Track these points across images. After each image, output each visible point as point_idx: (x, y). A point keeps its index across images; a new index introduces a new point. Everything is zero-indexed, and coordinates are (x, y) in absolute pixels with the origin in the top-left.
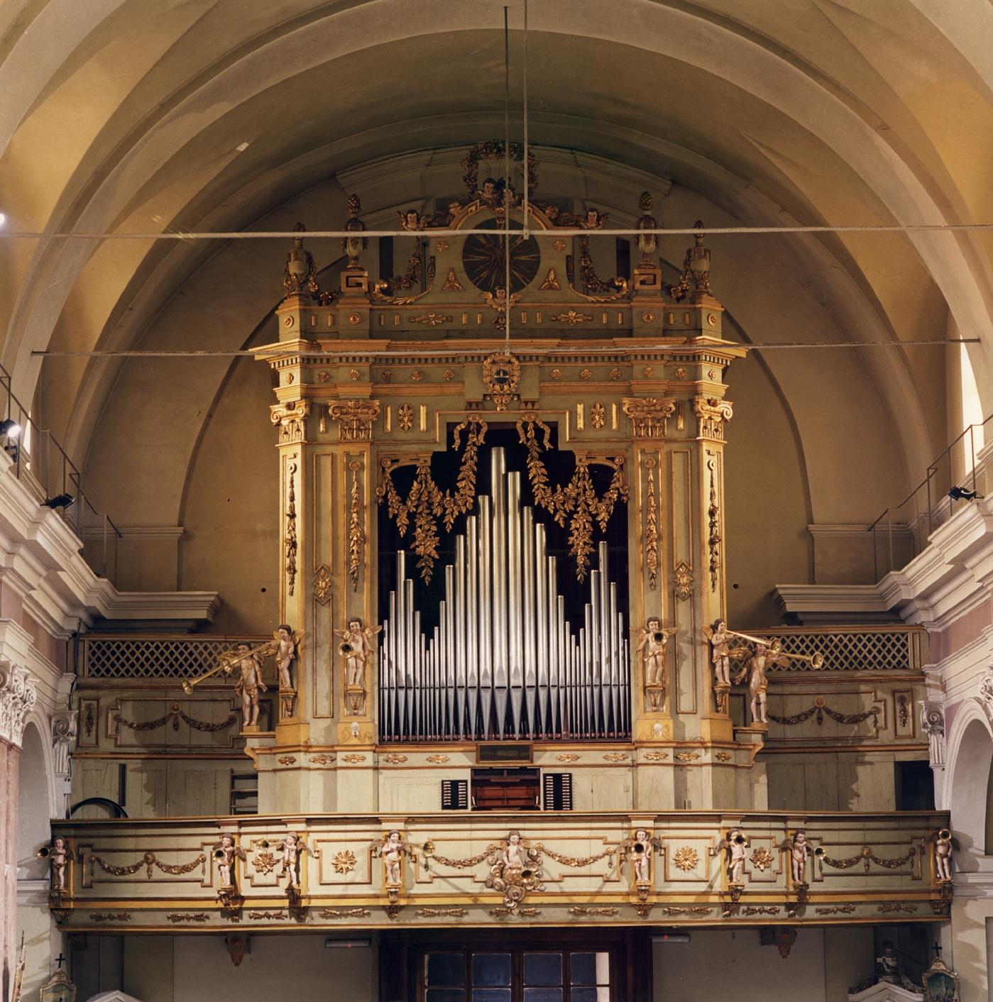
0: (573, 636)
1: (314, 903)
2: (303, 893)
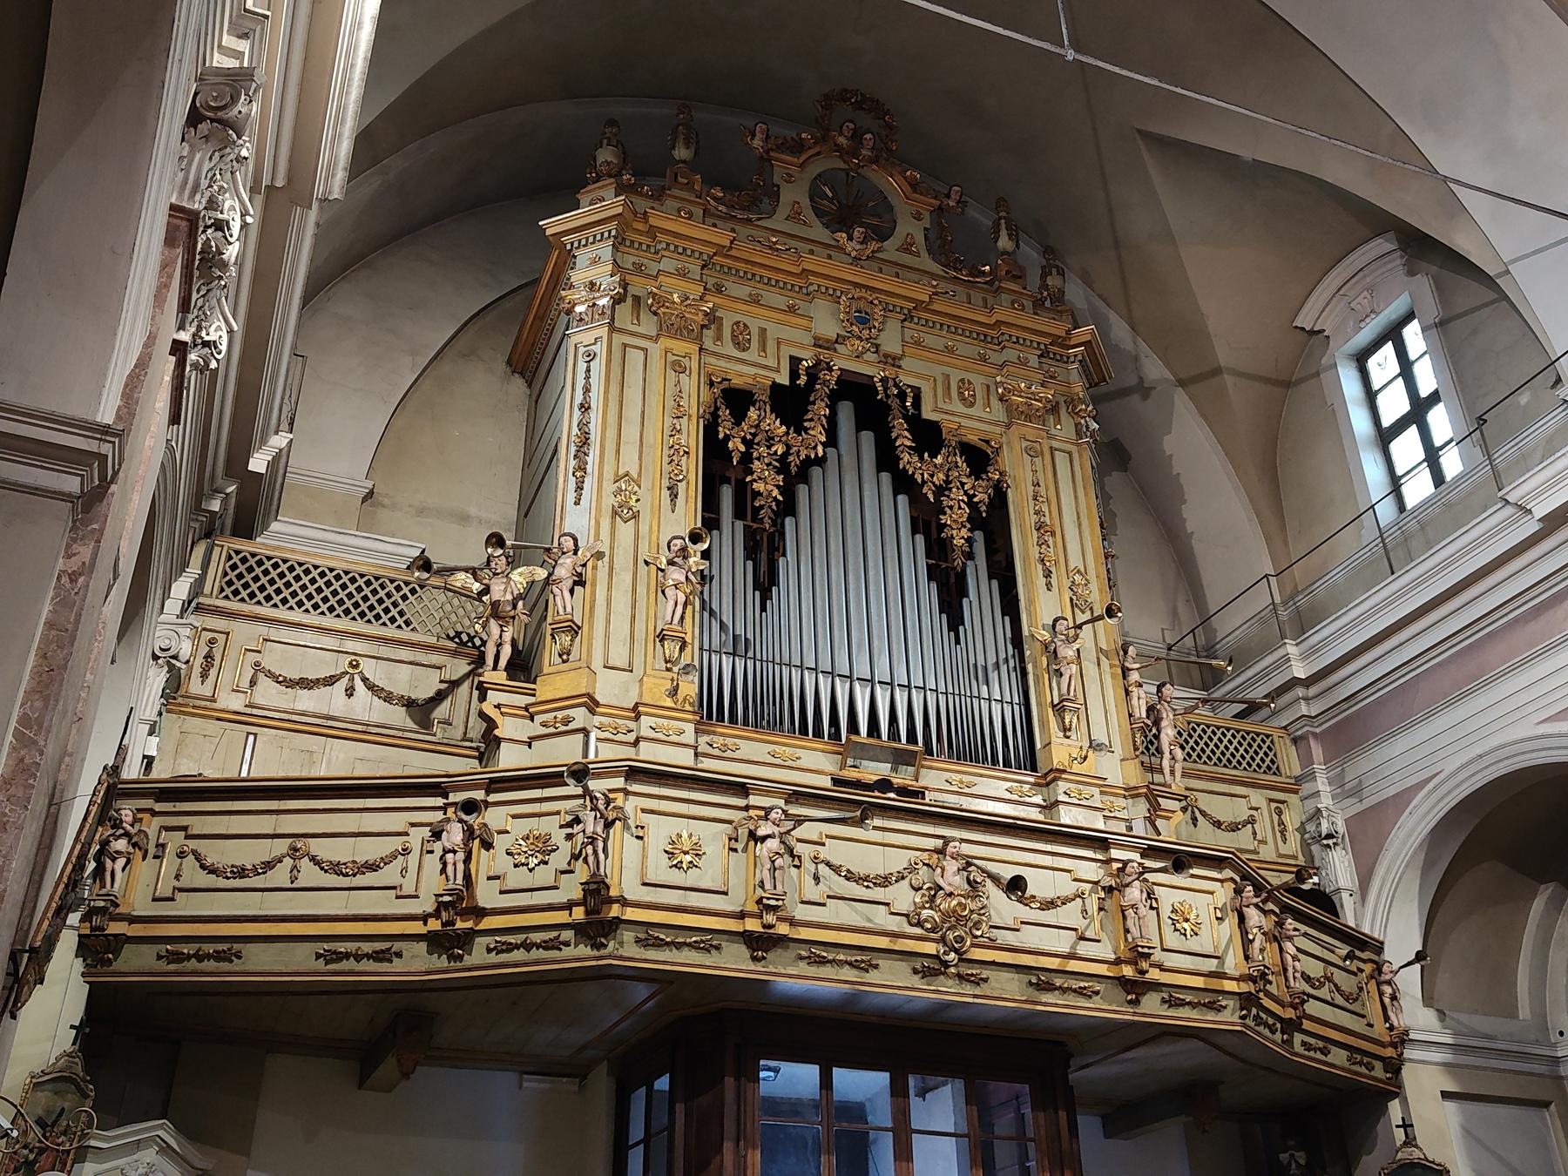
0: (952, 634)
1: (631, 914)
2: (613, 892)
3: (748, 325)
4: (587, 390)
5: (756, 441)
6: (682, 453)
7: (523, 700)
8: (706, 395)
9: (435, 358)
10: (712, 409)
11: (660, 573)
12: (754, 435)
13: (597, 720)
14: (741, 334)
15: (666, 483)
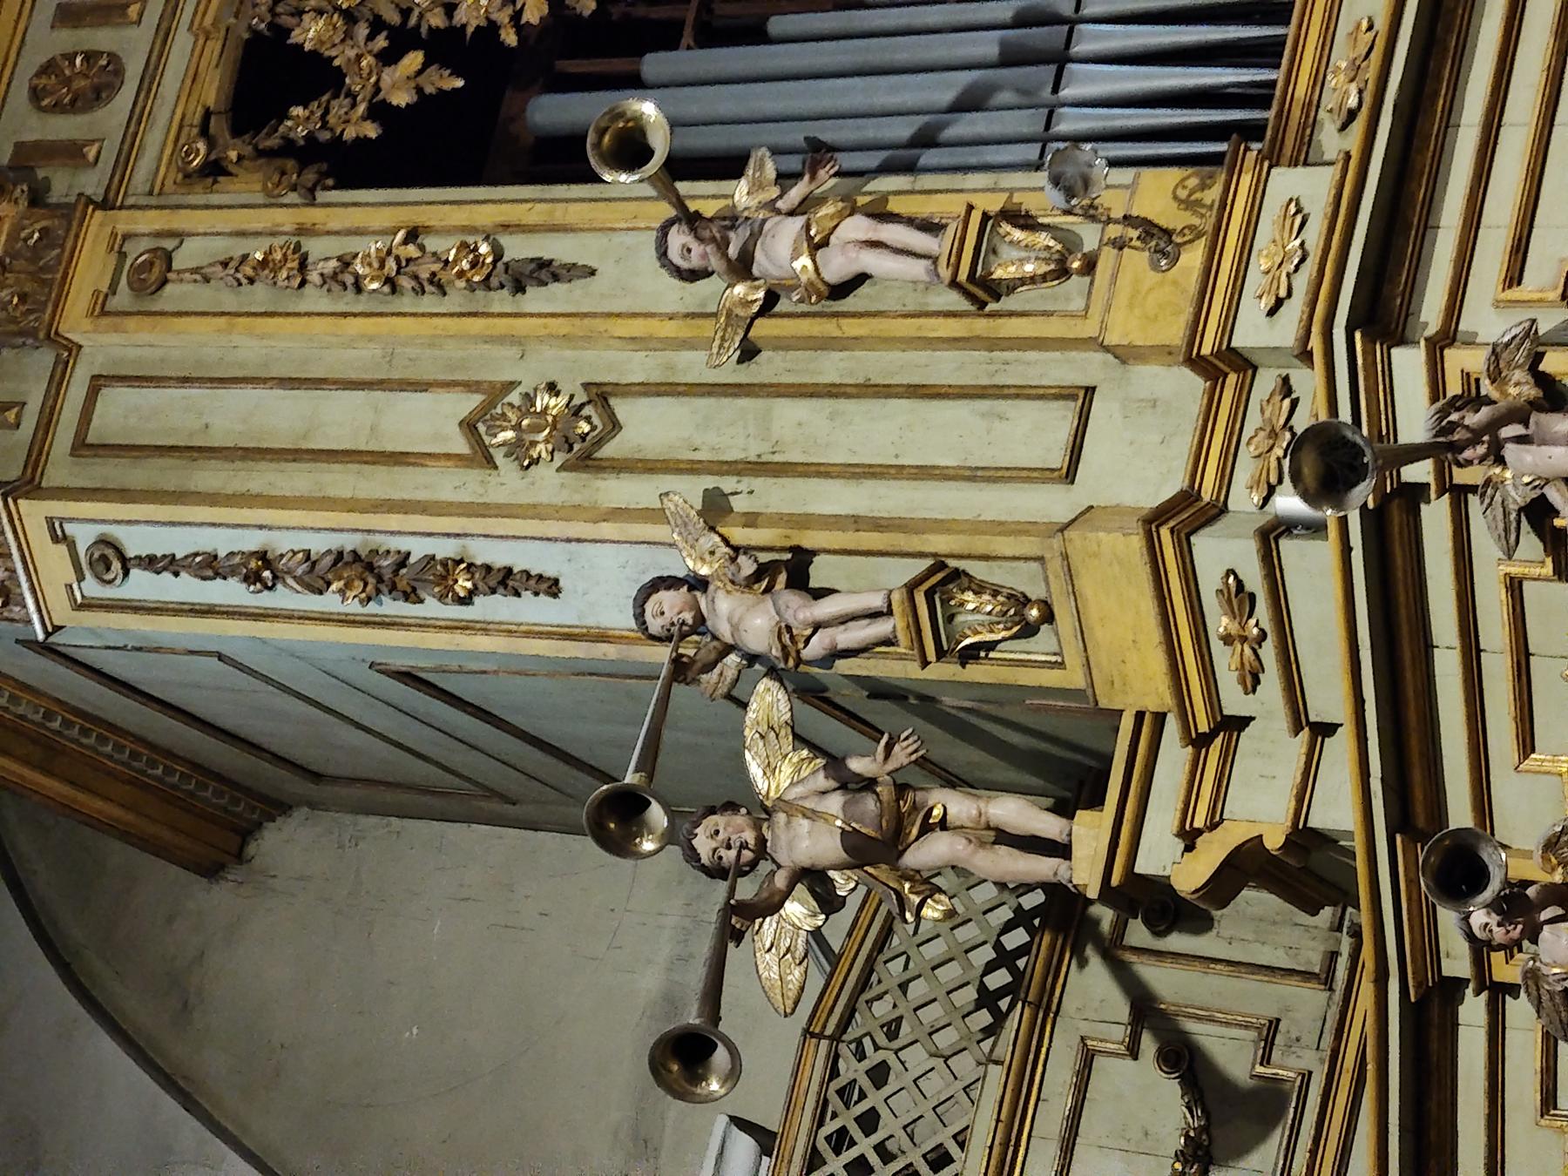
3: (43, 59)
4: (210, 566)
5: (393, 18)
6: (412, 251)
7: (1174, 757)
8: (246, 186)
9: (189, 1102)
10: (290, 164)
11: (782, 306)
12: (377, 25)
13: (1243, 498)
14: (67, 82)
15: (501, 300)
